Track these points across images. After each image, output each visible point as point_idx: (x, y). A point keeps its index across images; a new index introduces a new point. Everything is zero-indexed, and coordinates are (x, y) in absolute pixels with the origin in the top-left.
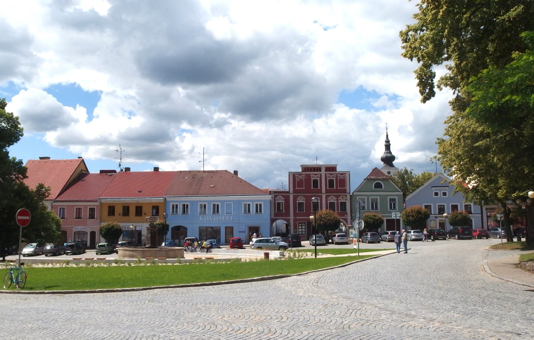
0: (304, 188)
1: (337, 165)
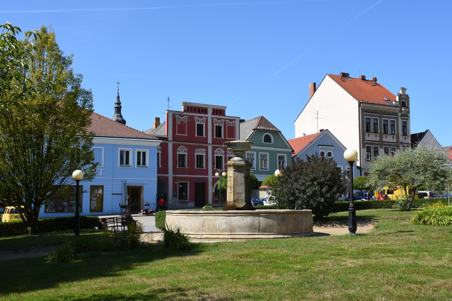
0: (186, 135)
1: (226, 107)
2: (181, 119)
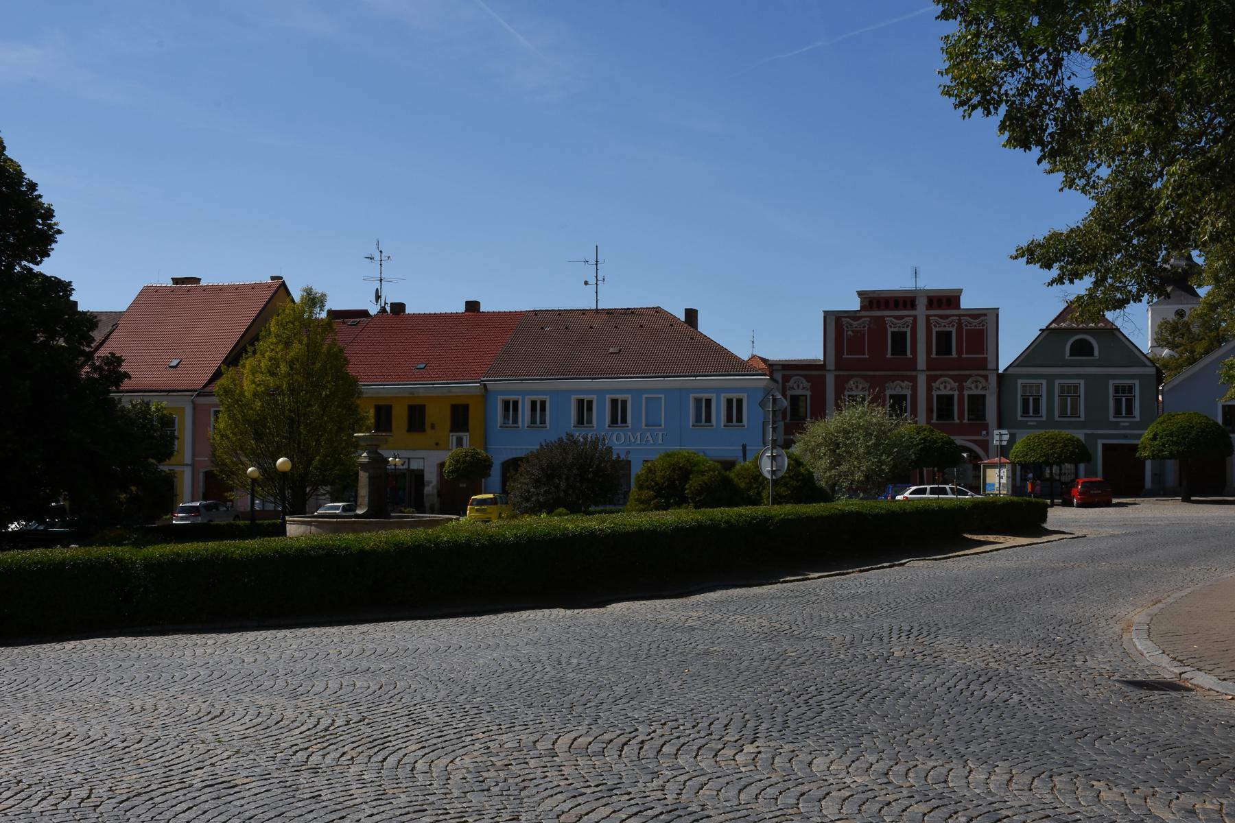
0: (867, 356)
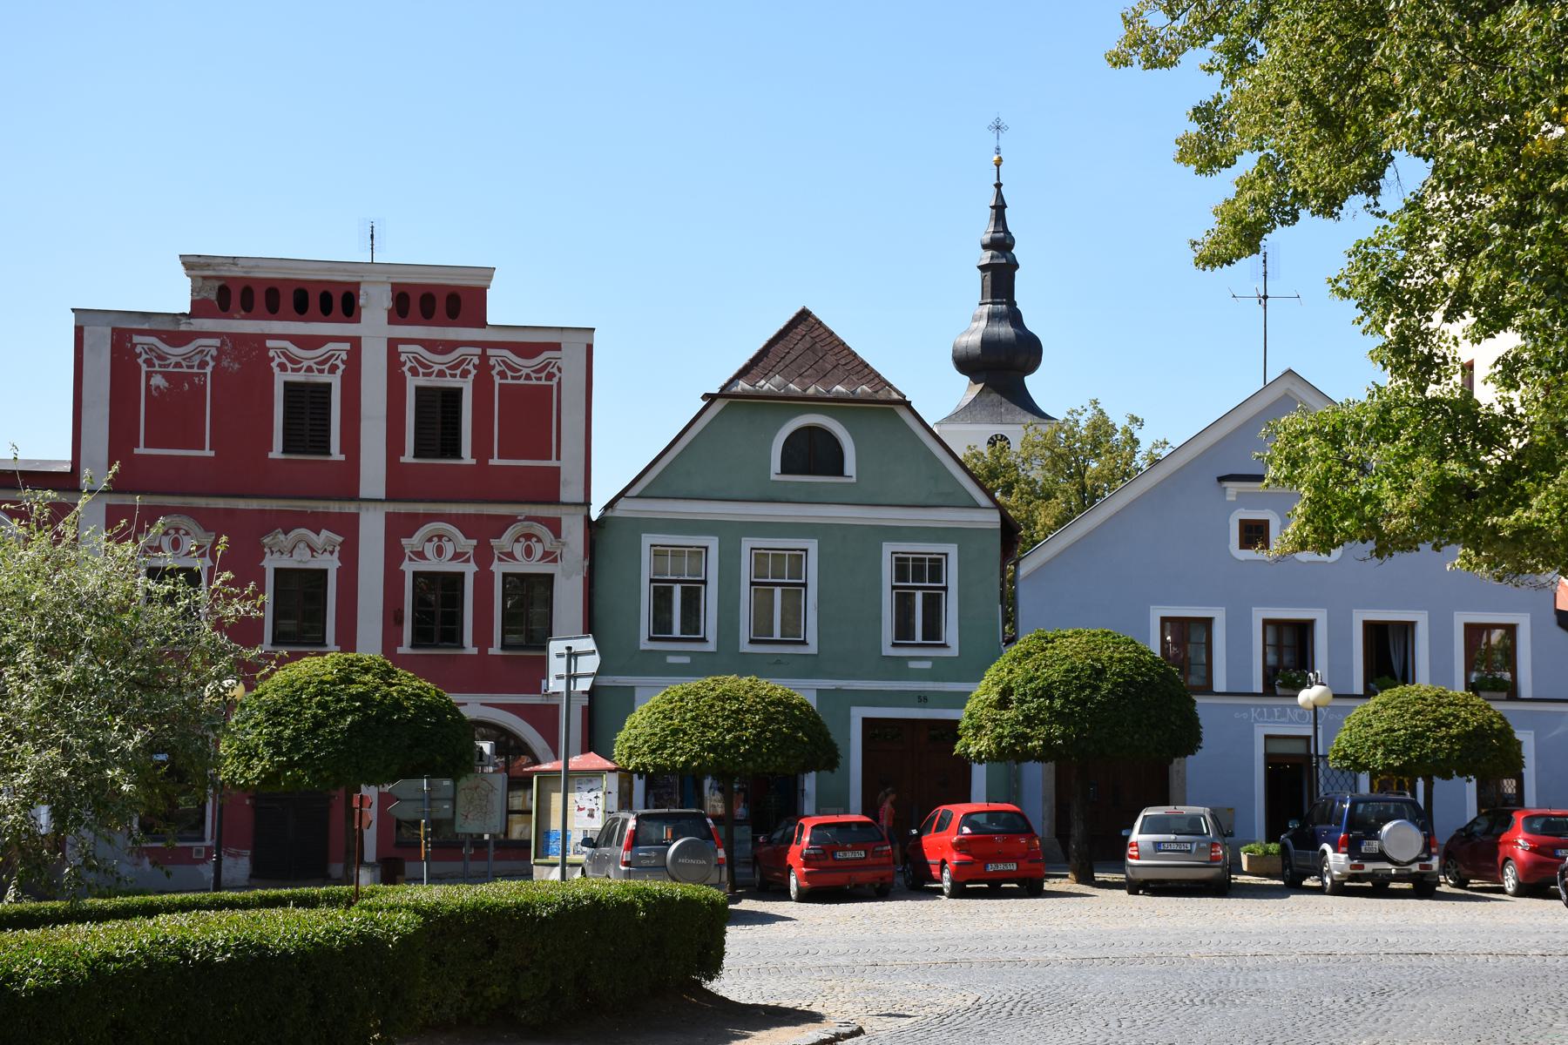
0: (208, 452)
1: (488, 273)
2: (173, 360)
